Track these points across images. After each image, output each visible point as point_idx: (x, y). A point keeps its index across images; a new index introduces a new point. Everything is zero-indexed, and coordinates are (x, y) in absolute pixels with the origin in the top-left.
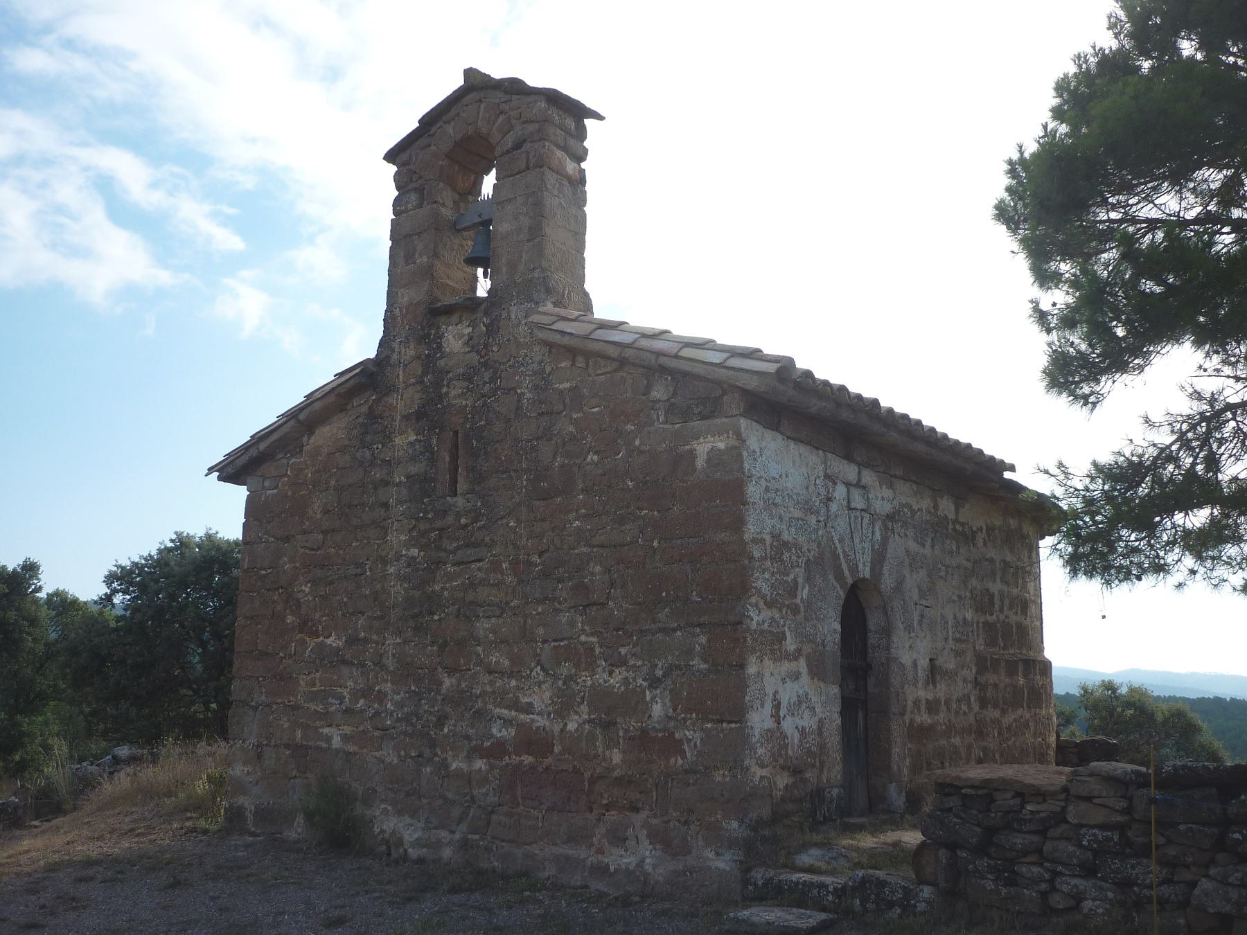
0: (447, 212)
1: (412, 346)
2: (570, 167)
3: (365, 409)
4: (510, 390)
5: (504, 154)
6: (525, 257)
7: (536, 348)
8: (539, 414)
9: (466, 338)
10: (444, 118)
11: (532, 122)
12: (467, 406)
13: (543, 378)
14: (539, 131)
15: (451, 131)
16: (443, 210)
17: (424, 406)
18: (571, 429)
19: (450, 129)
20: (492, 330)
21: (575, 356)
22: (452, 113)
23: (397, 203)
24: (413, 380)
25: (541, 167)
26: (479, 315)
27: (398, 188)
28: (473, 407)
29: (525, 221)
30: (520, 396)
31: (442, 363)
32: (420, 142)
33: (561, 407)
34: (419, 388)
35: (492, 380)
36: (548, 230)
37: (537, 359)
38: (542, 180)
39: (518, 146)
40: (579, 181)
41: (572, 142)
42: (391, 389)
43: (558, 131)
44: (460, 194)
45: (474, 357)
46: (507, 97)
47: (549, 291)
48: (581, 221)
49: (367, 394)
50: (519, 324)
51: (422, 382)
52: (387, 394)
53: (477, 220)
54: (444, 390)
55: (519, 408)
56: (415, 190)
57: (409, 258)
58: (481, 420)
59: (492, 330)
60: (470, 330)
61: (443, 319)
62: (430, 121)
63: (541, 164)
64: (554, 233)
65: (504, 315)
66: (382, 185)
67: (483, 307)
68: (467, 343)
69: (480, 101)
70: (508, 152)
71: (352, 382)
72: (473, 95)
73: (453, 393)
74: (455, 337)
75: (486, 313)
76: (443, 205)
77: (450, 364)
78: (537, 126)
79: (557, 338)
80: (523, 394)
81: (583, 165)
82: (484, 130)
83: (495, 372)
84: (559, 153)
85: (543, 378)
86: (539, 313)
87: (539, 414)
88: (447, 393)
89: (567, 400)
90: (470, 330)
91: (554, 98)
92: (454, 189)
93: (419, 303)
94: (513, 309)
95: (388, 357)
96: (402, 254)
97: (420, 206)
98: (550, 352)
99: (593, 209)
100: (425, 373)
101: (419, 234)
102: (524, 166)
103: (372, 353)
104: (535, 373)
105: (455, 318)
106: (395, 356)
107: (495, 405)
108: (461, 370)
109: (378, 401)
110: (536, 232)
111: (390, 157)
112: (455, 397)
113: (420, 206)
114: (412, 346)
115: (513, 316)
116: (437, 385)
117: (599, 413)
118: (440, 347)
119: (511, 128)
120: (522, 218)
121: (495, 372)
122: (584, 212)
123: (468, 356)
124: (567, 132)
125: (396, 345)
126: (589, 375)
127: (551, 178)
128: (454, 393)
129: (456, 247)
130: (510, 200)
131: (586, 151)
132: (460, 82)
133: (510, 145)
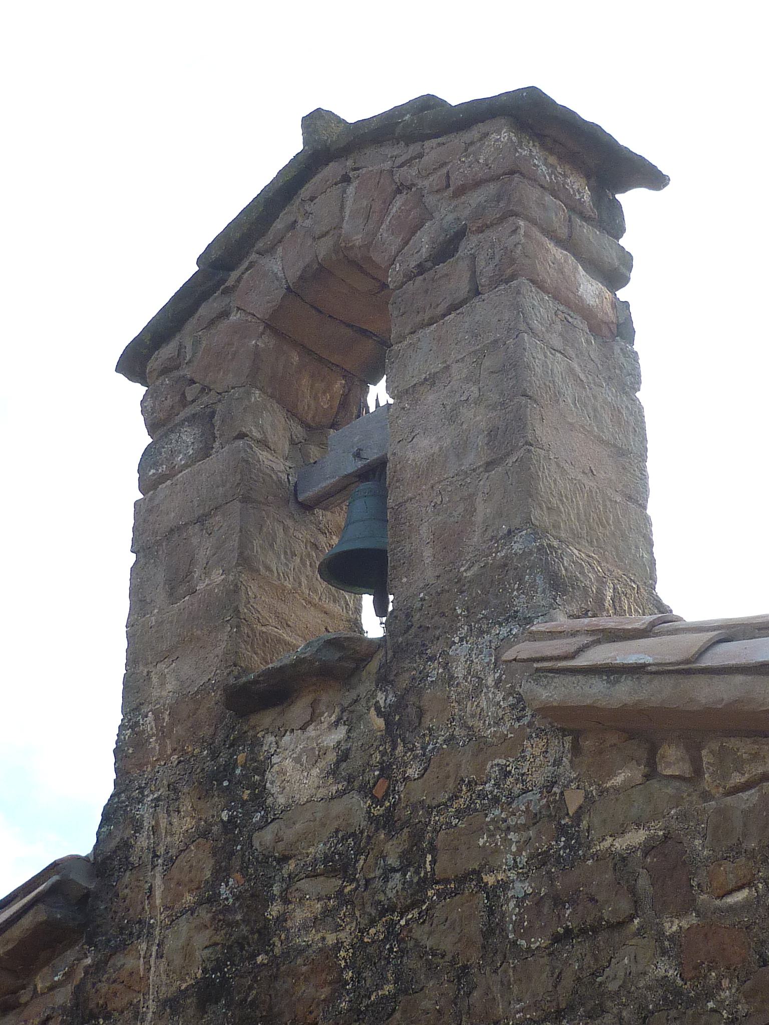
0: (275, 463)
1: (186, 805)
2: (589, 289)
3: (63, 997)
4: (462, 879)
5: (410, 277)
6: (483, 510)
7: (534, 748)
8: (557, 939)
9: (332, 757)
10: (260, 245)
11: (478, 184)
12: (338, 946)
13: (562, 830)
14: (498, 198)
15: (278, 267)
16: (263, 455)
17: (218, 967)
18: (665, 969)
19: (274, 265)
20: (401, 722)
21: (653, 751)
22: (279, 225)
23: (148, 459)
24: (189, 898)
25: (513, 277)
26: (365, 687)
27: (152, 427)
28: (359, 946)
29: (476, 418)
30: (494, 893)
31: (266, 837)
32: (205, 311)
33: (625, 906)
34: (204, 914)
35: (409, 860)
36: (542, 432)
37: (538, 778)
38: (518, 308)
39: (445, 251)
40: (617, 329)
41: (587, 232)
42: (132, 930)
43: (549, 199)
44: (307, 427)
45: (357, 806)
46: (414, 149)
47: (558, 585)
48: (632, 424)
49: (70, 955)
50: (479, 688)
51: (212, 899)
52: (122, 947)
53: (352, 466)
54: (275, 910)
55: (493, 928)
56: (192, 419)
57: (179, 582)
58: (384, 980)
59: (401, 722)
60: (340, 733)
61: (267, 718)
62: (225, 259)
63: (509, 272)
64: (561, 444)
65: (435, 671)
66: (120, 422)
67: (373, 666)
68: (333, 772)
69: (346, 179)
70: (421, 269)
71: (27, 922)
72: (332, 170)
73: (300, 915)
74: (299, 763)
75: (383, 680)
76: (264, 444)
77: (289, 835)
78: (492, 188)
79: (595, 691)
80: (504, 885)
81: (622, 294)
82: (358, 239)
83: (417, 837)
84: (558, 253)
85: (562, 830)
86: (534, 637)
87: (557, 939)
88: (282, 919)
89: (643, 882)
90: (340, 733)
91: (530, 114)
92: (292, 412)
93: (204, 689)
94: (460, 651)
95: (126, 845)
96: (161, 577)
97: (205, 452)
98: (576, 749)
99: (657, 397)
100: (221, 874)
101: (201, 520)
102: (463, 287)
103: (83, 844)
104: (535, 819)
105: (299, 710)
106: (143, 841)
107: (419, 932)
108: (318, 849)
109: (99, 968)
110: (509, 443)
111: (135, 362)
112: (305, 927)
113: (205, 452)
114: (186, 805)
115: (459, 671)
116: (255, 899)
117: (746, 905)
118: (260, 795)
119: (427, 215)
120: (467, 413)
121: (417, 837)
122: (635, 401)
123: (338, 807)
124: (575, 208)
125: (144, 812)
126: (706, 796)
127: (540, 309)
128: (305, 918)
129: (300, 548)
130: (431, 381)
131: (627, 260)
132: (292, 144)
133: (425, 251)
